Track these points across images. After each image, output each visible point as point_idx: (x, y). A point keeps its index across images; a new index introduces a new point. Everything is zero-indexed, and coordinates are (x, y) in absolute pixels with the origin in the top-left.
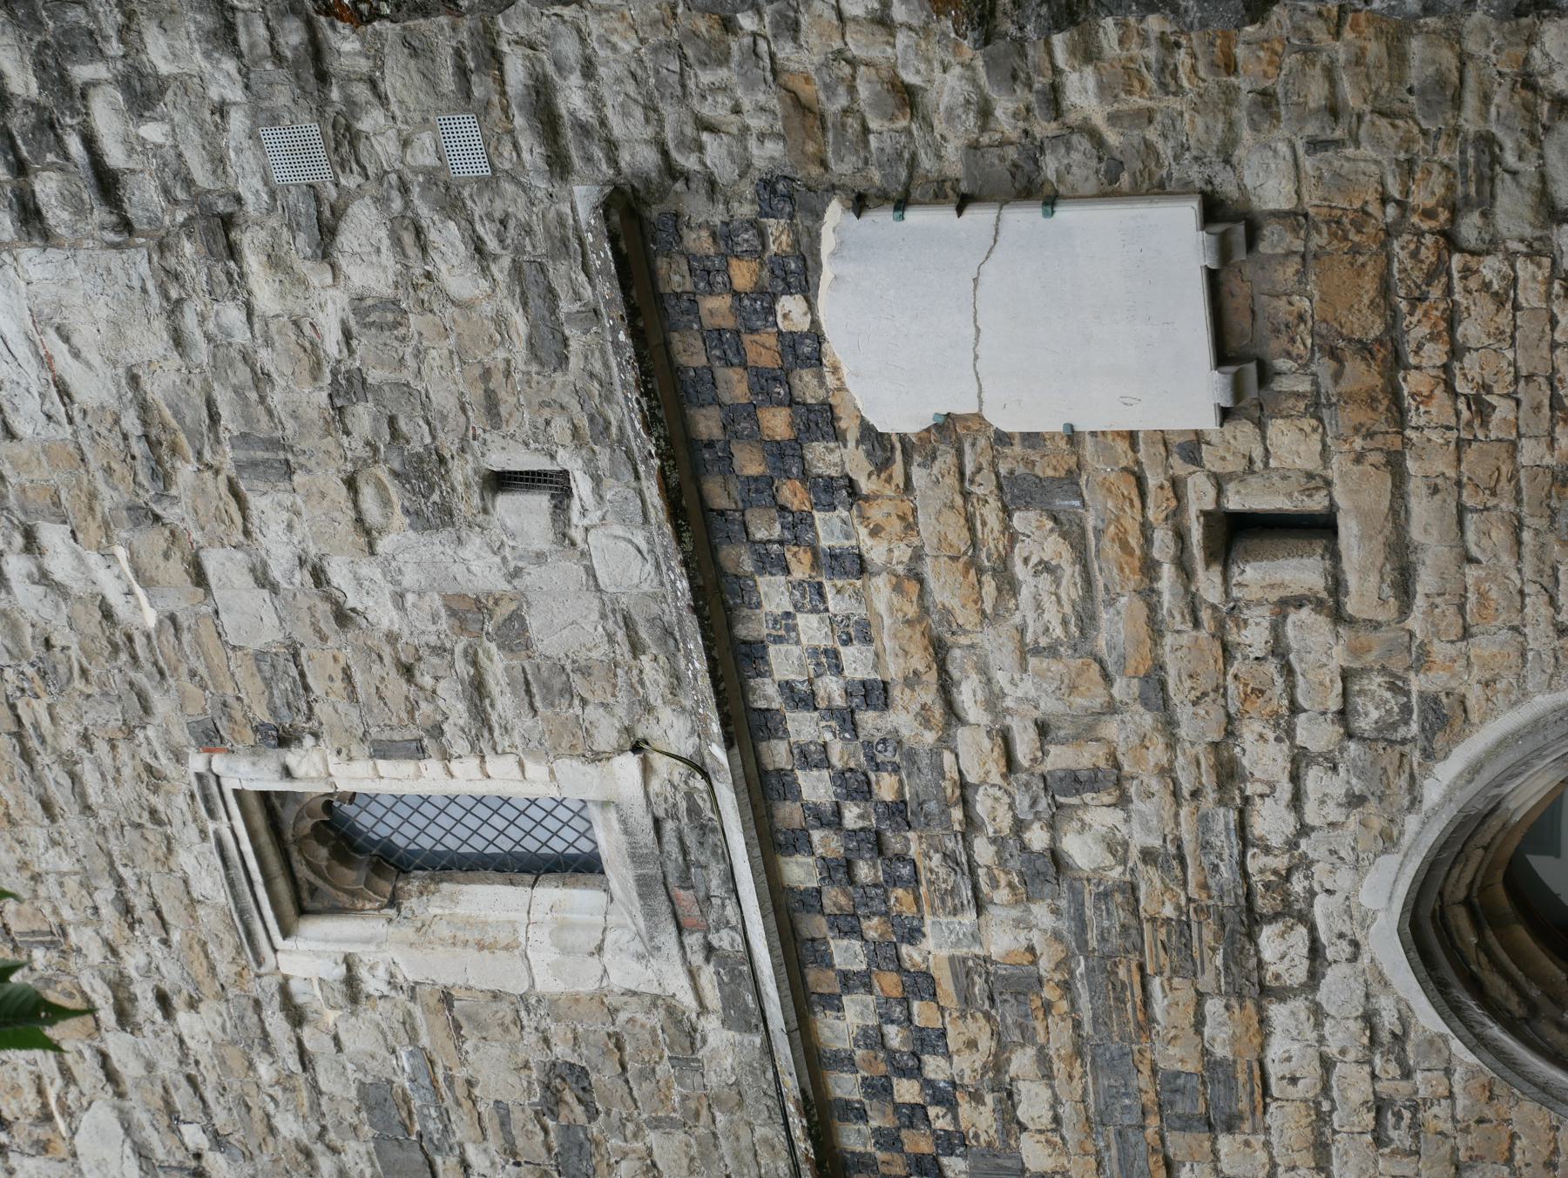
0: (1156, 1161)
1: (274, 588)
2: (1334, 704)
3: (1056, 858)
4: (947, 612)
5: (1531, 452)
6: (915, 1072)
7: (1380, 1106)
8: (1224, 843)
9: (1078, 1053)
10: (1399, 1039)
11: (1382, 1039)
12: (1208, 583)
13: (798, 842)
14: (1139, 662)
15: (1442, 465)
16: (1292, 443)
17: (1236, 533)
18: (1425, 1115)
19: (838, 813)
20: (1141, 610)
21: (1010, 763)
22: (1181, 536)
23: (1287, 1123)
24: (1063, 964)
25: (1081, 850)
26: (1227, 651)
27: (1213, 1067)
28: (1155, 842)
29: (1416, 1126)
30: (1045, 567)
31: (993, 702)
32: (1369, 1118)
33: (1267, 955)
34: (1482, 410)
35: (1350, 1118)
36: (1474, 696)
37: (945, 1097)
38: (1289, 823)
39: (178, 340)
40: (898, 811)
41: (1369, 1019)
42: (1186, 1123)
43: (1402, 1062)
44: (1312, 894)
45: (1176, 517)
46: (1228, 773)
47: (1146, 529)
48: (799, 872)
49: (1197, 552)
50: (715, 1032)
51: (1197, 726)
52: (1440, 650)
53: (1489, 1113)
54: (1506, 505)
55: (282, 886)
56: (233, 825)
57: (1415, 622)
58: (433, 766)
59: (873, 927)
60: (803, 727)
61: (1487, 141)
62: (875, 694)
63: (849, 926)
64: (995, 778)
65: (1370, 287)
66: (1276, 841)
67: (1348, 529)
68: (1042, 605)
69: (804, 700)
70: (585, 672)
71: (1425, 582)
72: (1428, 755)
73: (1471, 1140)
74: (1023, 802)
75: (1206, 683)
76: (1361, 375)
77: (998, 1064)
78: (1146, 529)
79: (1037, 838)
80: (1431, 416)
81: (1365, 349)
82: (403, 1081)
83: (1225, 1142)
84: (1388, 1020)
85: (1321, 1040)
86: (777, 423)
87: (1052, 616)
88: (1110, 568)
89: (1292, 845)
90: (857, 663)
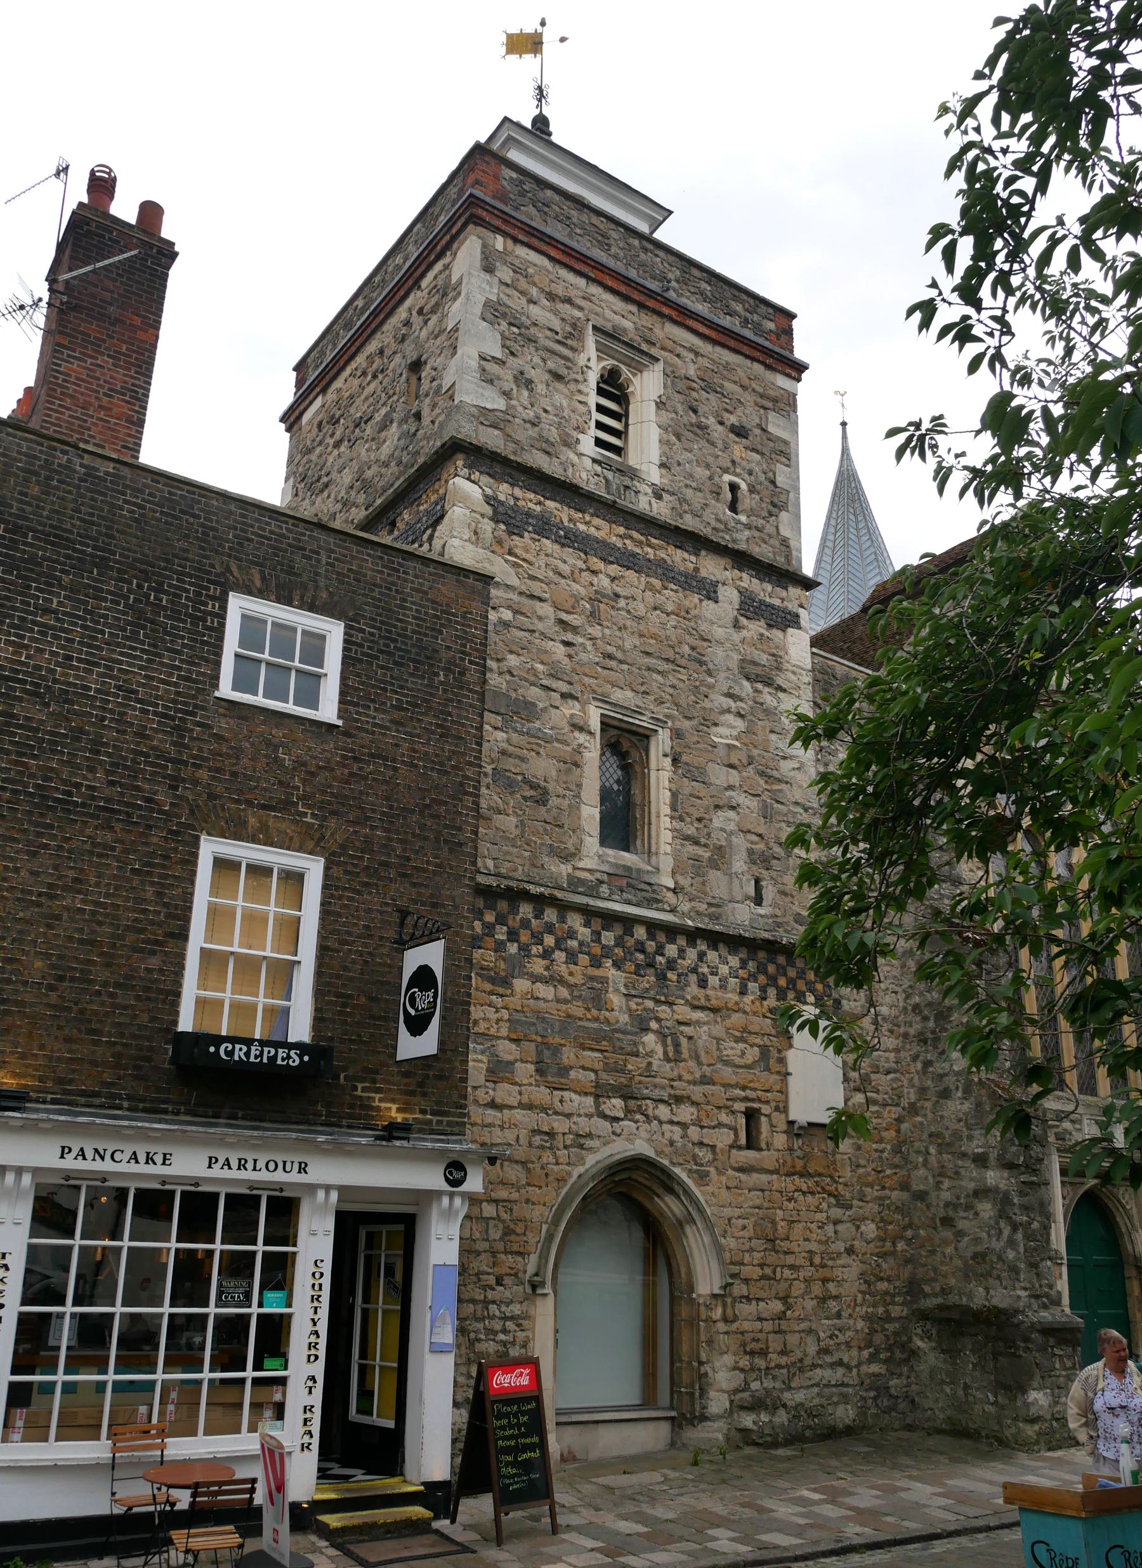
0: (521, 1035)
1: (726, 789)
2: (705, 1141)
3: (647, 1030)
4: (729, 1017)
5: (780, 1213)
6: (558, 945)
7: (551, 1134)
8: (657, 1093)
9: (569, 1016)
10: (581, 1146)
11: (580, 1141)
12: (740, 1106)
13: (651, 936)
14: (716, 1078)
15: (776, 1186)
16: (780, 1140)
17: (751, 1116)
18: (548, 1153)
19: (662, 955)
20: (733, 1082)
21: (680, 1023)
22: (752, 1100)
23: (541, 1094)
24: (607, 1021)
25: (650, 1039)
26: (719, 1108)
27: (564, 1071)
28: (655, 1068)
29: (543, 1147)
30: (743, 1053)
31: (698, 1023)
32: (546, 1129)
33: (613, 1101)
34: (790, 1200)
35: (546, 1122)
36: (709, 1189)
37: (546, 954)
38: (664, 1118)
39: (797, 803)
40: (662, 977)
41: (589, 1135)
42: (539, 1053)
43: (571, 1146)
44: (636, 1122)
45: (759, 1100)
46: (679, 1100)
47: (755, 1090)
48: (640, 932)
49: (749, 1104)
50: (565, 869)
51: (697, 1092)
52: (724, 1179)
53: (551, 1178)
54: (766, 1205)
55: (616, 723)
56: (644, 722)
57: (730, 1172)
58: (668, 811)
59: (618, 951)
60: (692, 954)
61: (850, 1207)
62: (703, 983)
63: (619, 942)
64: (676, 1017)
65: (821, 1170)
66: (657, 1112)
67: (751, 1154)
68: (732, 1050)
69: (701, 956)
70: (704, 883)
71: (743, 1177)
72: (690, 1171)
73: (538, 1170)
74: (668, 1024)
75: (710, 1098)
76: (799, 1164)
77: (562, 981)
78: (755, 1090)
79: (654, 1025)
80: (789, 1184)
81: (805, 1166)
82: (537, 724)
83: (531, 1068)
84: (589, 1143)
85: (579, 1115)
86: (782, 982)
87: (729, 1052)
88: (743, 1076)
89: (656, 1118)
90: (713, 981)
